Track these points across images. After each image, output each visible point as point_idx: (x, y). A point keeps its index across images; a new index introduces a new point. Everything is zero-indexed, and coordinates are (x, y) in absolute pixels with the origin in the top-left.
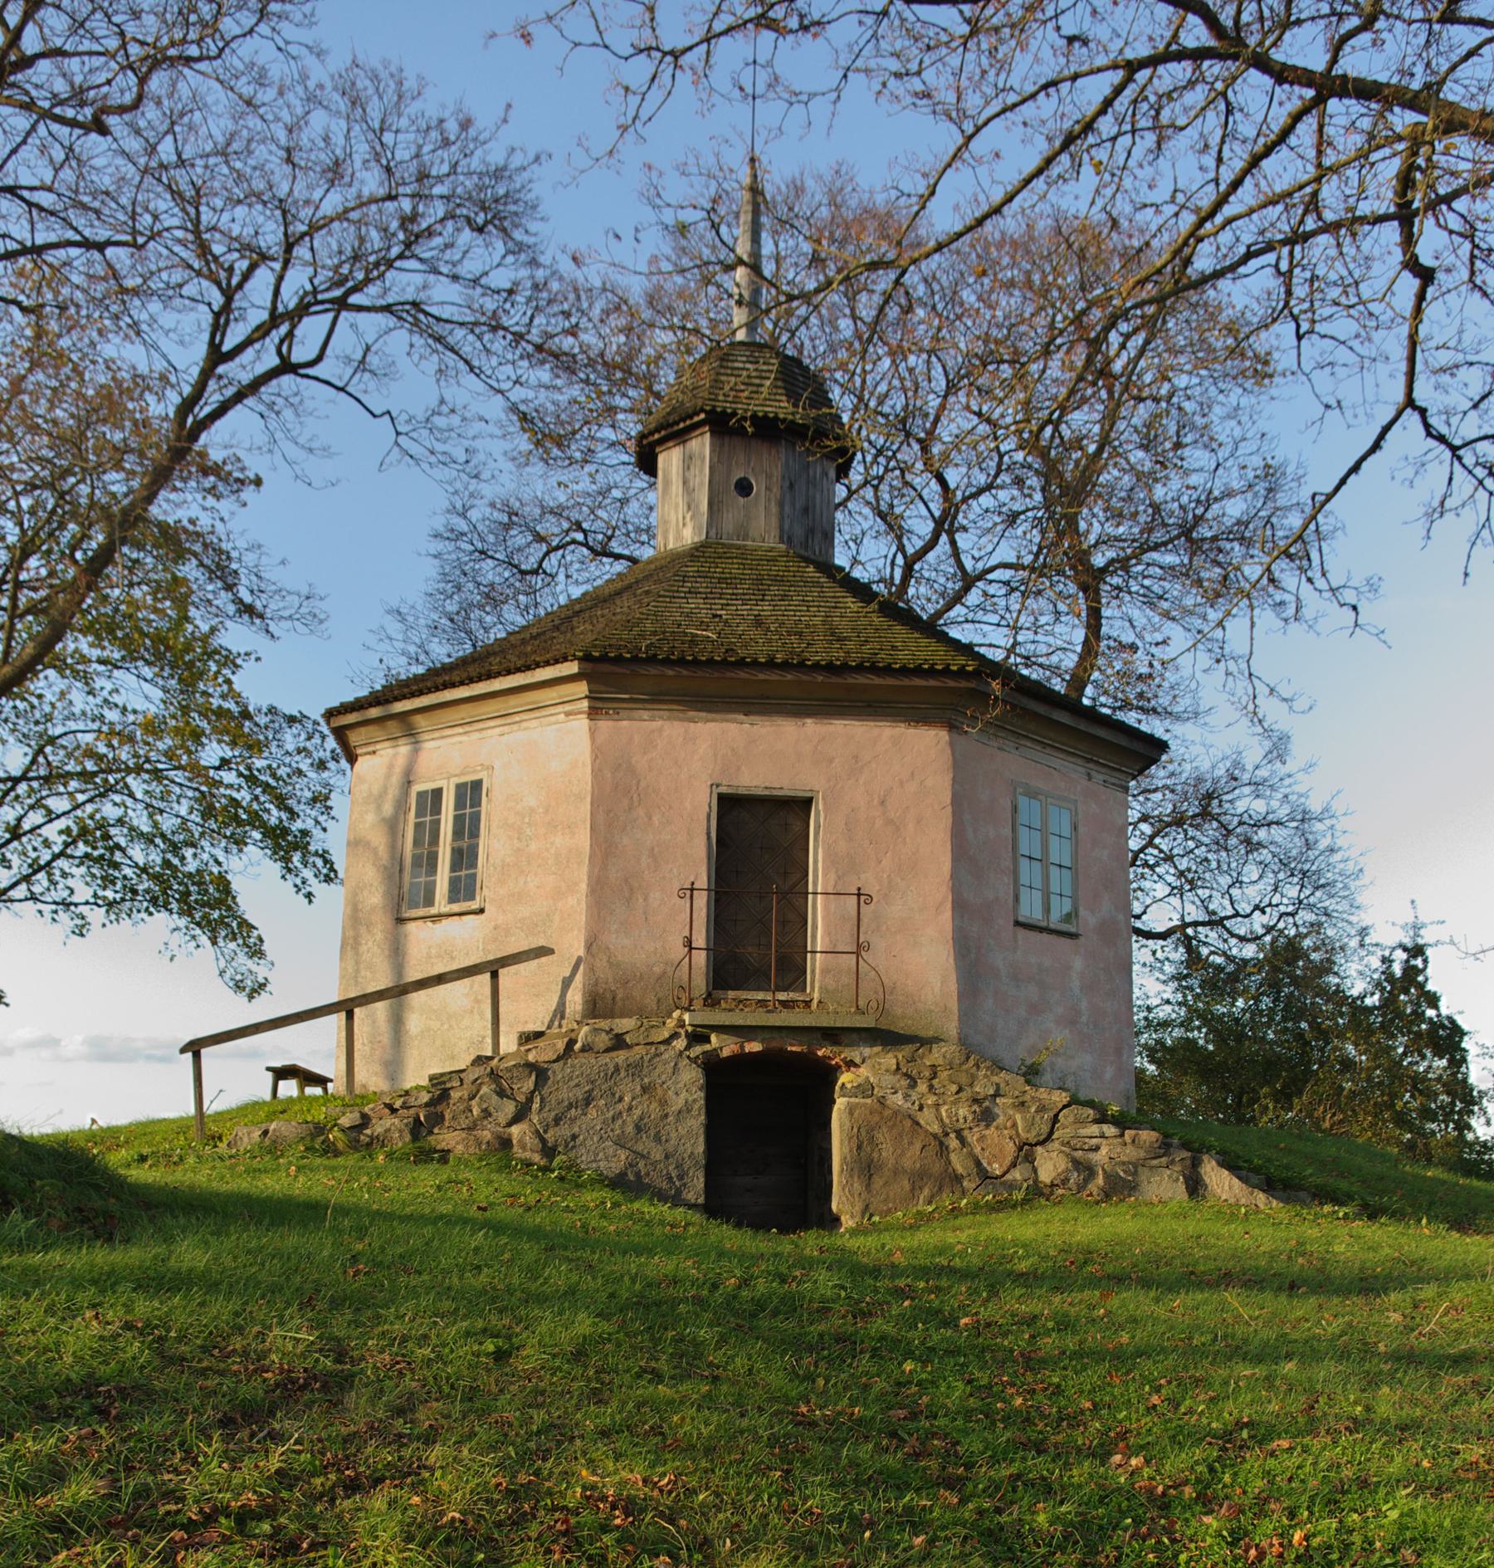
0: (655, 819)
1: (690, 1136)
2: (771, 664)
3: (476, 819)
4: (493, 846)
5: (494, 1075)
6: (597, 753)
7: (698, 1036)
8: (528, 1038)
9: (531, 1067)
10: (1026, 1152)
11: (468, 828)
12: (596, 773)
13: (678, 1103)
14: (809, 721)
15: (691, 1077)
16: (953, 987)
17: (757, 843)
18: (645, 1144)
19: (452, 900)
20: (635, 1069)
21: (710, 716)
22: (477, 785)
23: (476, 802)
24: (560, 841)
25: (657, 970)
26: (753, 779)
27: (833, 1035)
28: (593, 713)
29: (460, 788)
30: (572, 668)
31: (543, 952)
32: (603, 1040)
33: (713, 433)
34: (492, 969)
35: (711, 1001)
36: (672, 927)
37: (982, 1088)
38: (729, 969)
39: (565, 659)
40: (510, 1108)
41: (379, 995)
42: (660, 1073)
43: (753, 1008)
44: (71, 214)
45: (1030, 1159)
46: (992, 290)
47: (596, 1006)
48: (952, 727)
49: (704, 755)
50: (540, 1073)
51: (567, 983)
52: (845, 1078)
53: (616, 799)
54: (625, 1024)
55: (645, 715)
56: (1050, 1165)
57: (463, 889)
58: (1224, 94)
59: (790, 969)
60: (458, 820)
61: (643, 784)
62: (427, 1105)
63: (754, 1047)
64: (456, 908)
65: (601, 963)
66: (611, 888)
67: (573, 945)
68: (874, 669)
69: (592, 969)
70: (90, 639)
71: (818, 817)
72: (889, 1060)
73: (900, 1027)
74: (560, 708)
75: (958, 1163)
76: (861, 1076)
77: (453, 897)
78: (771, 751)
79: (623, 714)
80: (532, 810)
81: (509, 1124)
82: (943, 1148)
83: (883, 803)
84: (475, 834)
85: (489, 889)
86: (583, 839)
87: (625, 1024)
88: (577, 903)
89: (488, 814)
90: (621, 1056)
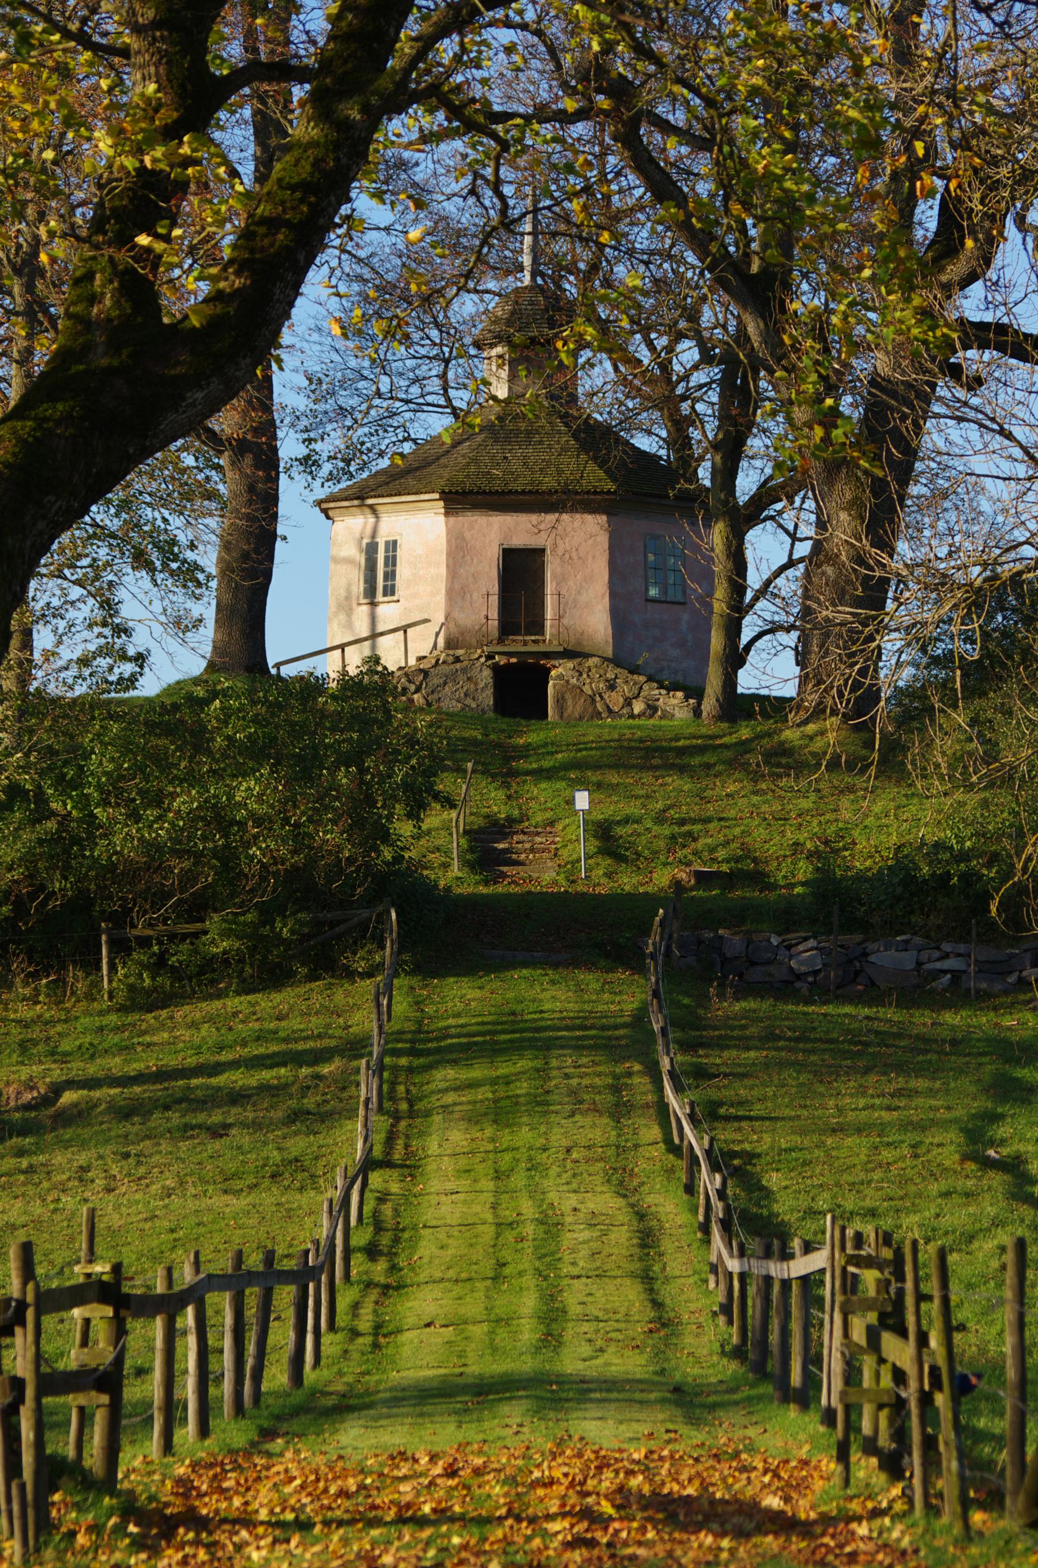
1: (487, 698)
2: (523, 492)
3: (394, 557)
4: (403, 571)
5: (406, 675)
6: (449, 532)
7: (490, 657)
8: (420, 659)
9: (421, 671)
10: (628, 702)
11: (391, 561)
12: (449, 541)
13: (481, 685)
15: (487, 673)
16: (610, 631)
17: (521, 574)
18: (468, 701)
19: (385, 595)
20: (464, 670)
22: (395, 542)
23: (395, 550)
24: (433, 571)
26: (520, 540)
27: (547, 655)
28: (447, 514)
29: (387, 543)
30: (437, 496)
31: (426, 621)
32: (451, 659)
34: (405, 629)
35: (501, 641)
36: (484, 609)
37: (610, 675)
38: (508, 627)
40: (413, 688)
41: (365, 639)
42: (474, 672)
43: (518, 644)
45: (630, 704)
47: (450, 644)
48: (608, 514)
49: (496, 531)
50: (425, 673)
51: (437, 634)
52: (553, 673)
53: (458, 552)
54: (460, 652)
56: (638, 707)
58: (447, 362)
59: (537, 626)
60: (386, 558)
63: (514, 660)
65: (452, 625)
66: (457, 591)
67: (439, 618)
68: (595, 493)
70: (113, 977)
71: (549, 556)
72: (570, 665)
73: (586, 650)
75: (600, 707)
76: (561, 671)
78: (520, 529)
82: (593, 701)
84: (394, 564)
85: (400, 592)
86: (443, 571)
87: (460, 652)
88: (441, 599)
90: (458, 666)
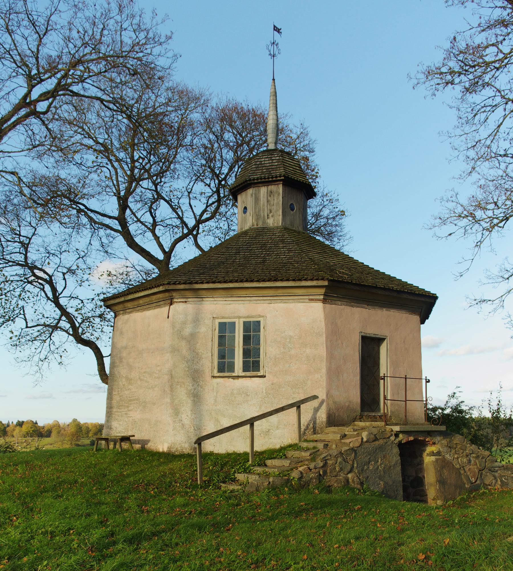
0: (344, 344)
6: (326, 317)
14: (384, 309)
21: (358, 305)
25: (347, 404)
33: (283, 184)
39: (323, 279)
44: (23, 67)
46: (254, 141)
55: (339, 303)
57: (252, 364)
61: (340, 330)
62: (322, 467)
64: (248, 374)
65: (331, 402)
66: (334, 373)
67: (322, 396)
69: (328, 404)
74: (307, 297)
77: (246, 368)
79: (333, 302)
80: (291, 337)
81: (348, 474)
83: (404, 342)
86: (322, 351)
89: (265, 336)
